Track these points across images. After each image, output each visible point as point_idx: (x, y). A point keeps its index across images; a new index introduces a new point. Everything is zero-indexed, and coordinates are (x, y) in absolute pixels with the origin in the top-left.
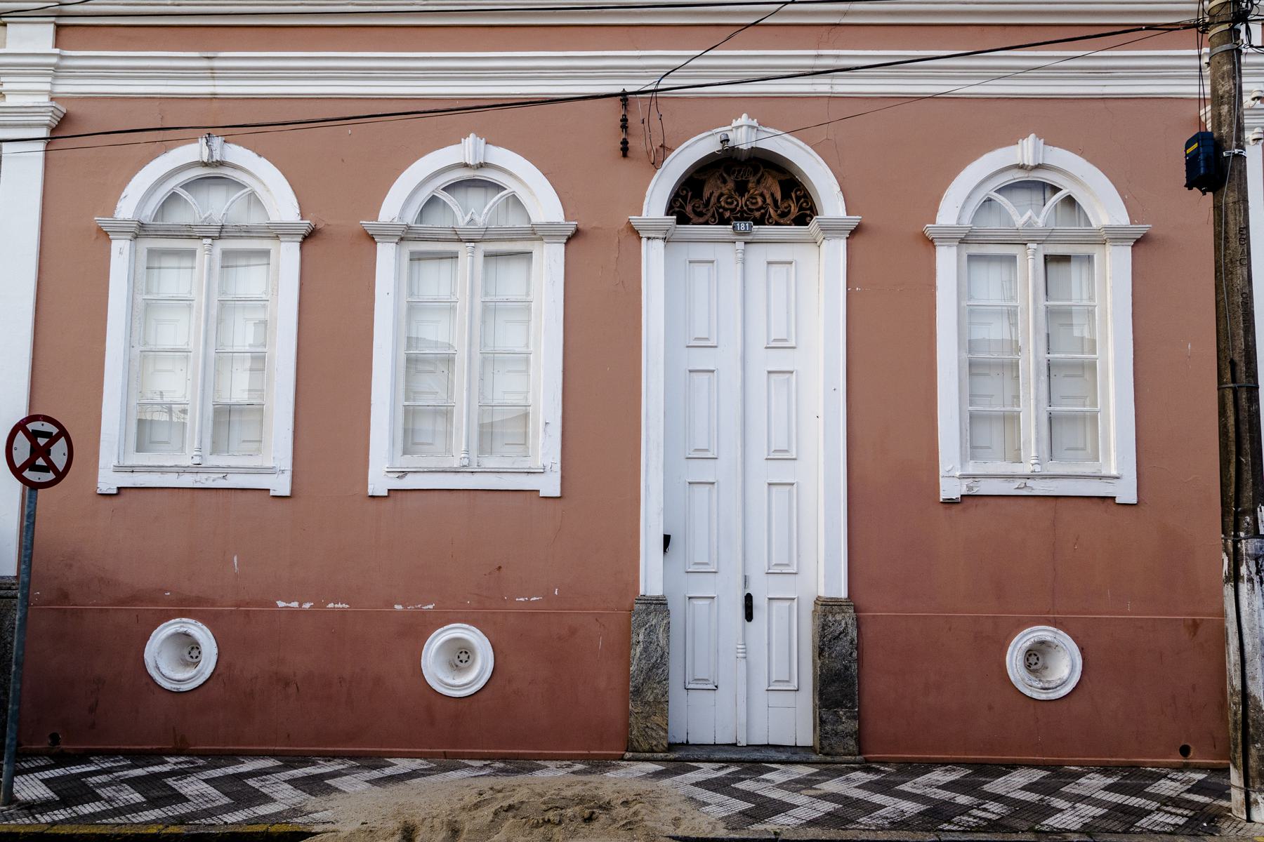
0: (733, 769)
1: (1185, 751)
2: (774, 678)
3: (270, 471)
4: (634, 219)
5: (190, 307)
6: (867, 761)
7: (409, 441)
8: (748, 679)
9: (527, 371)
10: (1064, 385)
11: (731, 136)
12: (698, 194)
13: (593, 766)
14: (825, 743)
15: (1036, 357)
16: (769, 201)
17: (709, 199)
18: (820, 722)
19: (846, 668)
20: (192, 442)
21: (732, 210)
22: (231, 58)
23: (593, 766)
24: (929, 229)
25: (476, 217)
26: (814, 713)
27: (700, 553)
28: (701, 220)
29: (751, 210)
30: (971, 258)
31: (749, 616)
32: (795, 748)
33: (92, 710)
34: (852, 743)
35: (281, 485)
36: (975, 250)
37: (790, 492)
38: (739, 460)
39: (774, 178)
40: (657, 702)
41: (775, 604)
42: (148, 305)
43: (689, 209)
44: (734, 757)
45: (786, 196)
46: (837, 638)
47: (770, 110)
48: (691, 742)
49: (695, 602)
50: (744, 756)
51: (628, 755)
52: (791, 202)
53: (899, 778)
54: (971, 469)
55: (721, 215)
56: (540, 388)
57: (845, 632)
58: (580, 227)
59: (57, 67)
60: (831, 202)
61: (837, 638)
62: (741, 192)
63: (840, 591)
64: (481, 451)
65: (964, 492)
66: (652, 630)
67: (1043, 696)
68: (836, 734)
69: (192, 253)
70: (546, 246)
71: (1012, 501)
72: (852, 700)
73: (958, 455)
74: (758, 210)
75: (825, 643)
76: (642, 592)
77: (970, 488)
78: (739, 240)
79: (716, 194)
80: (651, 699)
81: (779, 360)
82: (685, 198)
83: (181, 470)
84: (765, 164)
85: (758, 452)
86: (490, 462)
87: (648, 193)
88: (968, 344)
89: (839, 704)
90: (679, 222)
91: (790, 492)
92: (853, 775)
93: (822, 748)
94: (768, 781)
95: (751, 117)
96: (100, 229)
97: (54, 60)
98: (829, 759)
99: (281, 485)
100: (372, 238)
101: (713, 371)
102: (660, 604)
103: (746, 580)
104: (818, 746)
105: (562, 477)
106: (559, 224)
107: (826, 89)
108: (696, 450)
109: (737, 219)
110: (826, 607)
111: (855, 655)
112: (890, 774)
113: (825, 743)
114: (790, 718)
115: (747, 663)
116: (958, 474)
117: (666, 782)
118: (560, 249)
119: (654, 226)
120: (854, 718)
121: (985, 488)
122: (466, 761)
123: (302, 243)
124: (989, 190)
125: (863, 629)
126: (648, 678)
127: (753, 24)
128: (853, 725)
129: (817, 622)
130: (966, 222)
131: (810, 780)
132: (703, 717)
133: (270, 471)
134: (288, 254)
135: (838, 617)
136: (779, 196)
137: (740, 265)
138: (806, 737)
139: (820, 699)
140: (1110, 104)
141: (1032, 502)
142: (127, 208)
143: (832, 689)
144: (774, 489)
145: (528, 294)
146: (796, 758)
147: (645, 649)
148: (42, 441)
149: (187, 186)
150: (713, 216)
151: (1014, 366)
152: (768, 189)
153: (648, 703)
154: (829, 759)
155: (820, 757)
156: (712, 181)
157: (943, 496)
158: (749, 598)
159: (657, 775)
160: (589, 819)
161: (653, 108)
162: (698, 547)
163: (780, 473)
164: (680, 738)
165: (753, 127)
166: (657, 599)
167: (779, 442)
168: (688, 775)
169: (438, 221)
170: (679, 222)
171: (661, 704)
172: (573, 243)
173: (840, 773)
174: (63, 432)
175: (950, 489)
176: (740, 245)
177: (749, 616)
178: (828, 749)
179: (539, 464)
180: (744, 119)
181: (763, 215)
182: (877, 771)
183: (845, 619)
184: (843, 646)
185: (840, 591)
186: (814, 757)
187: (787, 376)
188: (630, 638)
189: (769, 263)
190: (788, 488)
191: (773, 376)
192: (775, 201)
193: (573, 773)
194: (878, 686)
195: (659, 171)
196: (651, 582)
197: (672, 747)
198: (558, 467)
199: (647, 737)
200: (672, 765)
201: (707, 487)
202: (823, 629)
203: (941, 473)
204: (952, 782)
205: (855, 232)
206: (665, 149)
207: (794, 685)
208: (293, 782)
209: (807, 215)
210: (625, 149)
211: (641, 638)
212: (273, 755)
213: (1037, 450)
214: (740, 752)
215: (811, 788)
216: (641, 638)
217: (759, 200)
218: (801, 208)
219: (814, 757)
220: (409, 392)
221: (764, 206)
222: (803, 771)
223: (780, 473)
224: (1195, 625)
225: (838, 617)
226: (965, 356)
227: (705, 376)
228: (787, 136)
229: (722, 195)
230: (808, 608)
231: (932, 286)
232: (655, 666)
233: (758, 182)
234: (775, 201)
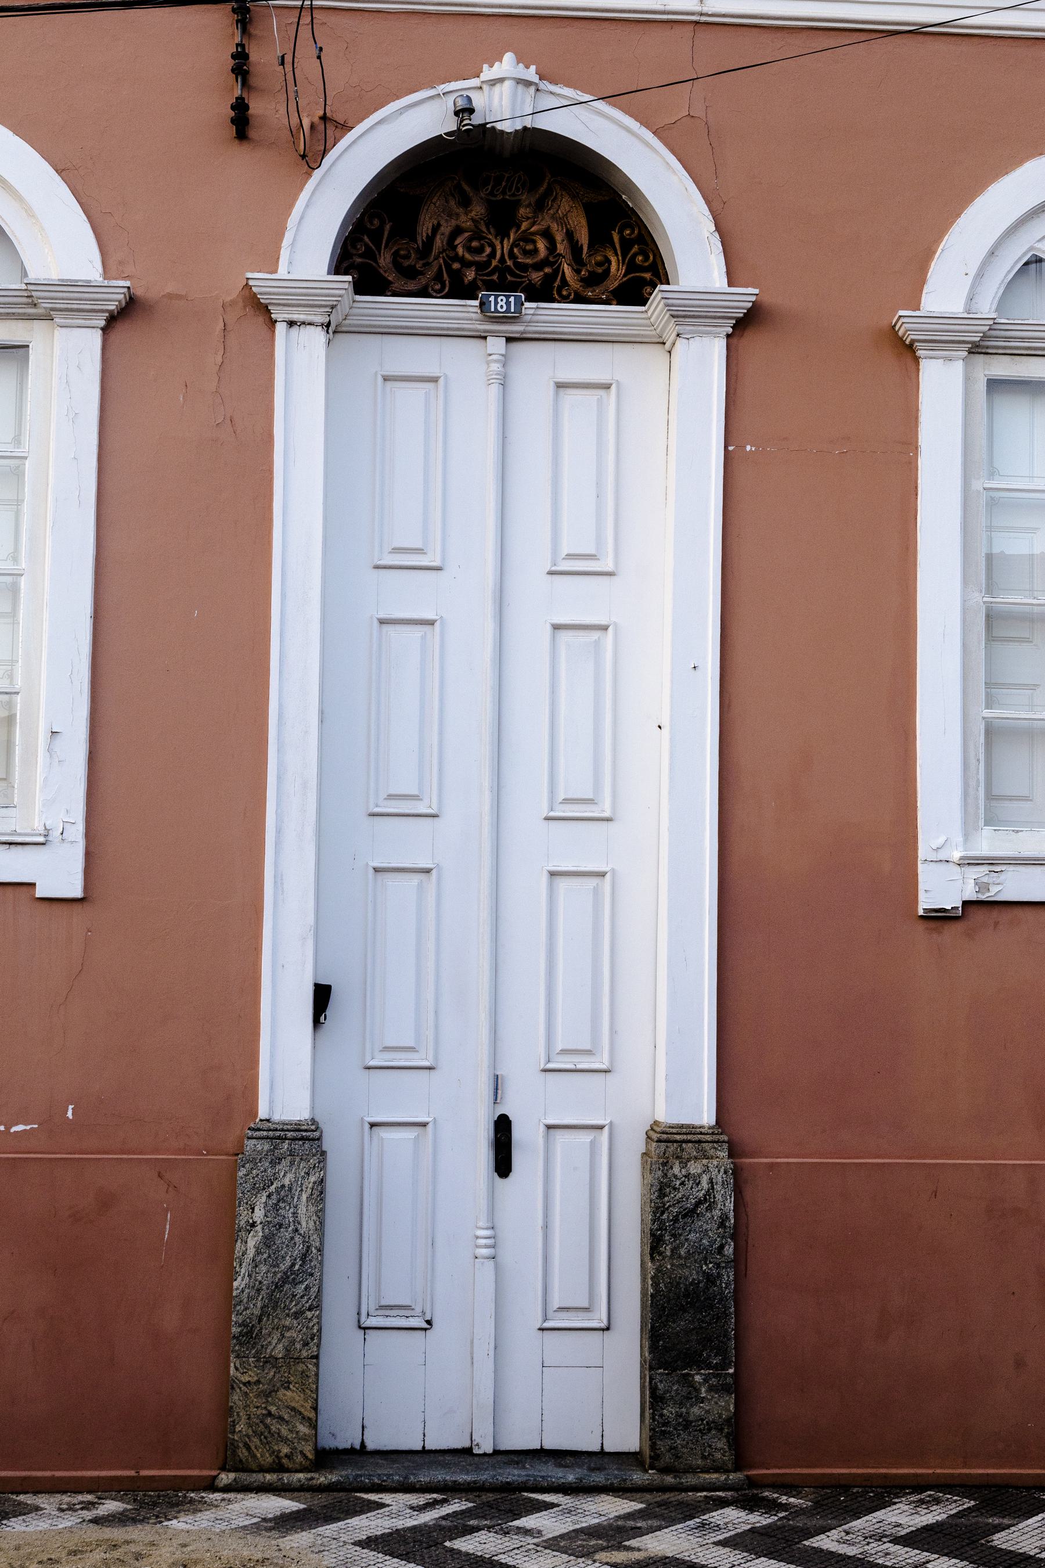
0: (456, 1506)
2: (556, 1302)
4: (259, 280)
6: (752, 1483)
7: (991, 802)
8: (496, 1306)
9: (14, 614)
10: (1023, 661)
11: (478, 101)
12: (406, 228)
13: (142, 1505)
14: (662, 1445)
16: (561, 248)
17: (431, 239)
18: (654, 1399)
19: (711, 1279)
21: (481, 267)
23: (142, 1505)
24: (907, 323)
26: (642, 1377)
27: (398, 1030)
28: (412, 286)
29: (524, 268)
30: (995, 385)
31: (503, 1165)
32: (601, 1457)
34: (721, 1444)
35: (60, 874)
36: (1003, 368)
37: (596, 892)
38: (487, 819)
39: (574, 197)
40: (291, 1358)
41: (561, 1138)
43: (385, 260)
44: (463, 1478)
45: (599, 238)
46: (691, 1213)
48: (371, 1446)
49: (384, 1133)
50: (484, 1477)
51: (226, 1478)
52: (618, 256)
53: (817, 1521)
54: (987, 844)
55: (456, 277)
57: (708, 1200)
58: (139, 292)
60: (696, 258)
61: (691, 1213)
62: (498, 228)
63: (702, 1111)
65: (970, 894)
66: (283, 1197)
68: (687, 1425)
70: (59, 333)
72: (722, 1351)
73: (957, 814)
74: (538, 267)
75: (667, 1222)
76: (263, 1113)
77: (982, 887)
78: (496, 334)
79: (446, 229)
80: (279, 1351)
81: (578, 602)
82: (376, 236)
85: (528, 803)
87: (292, 221)
88: (987, 569)
89: (695, 1361)
90: (361, 288)
91: (596, 892)
92: (716, 1517)
93: (655, 1457)
94: (527, 1532)
95: (523, 59)
98: (669, 1479)
100: (911, 348)
101: (431, 623)
102: (304, 1140)
103: (497, 1085)
104: (647, 1452)
105: (88, 855)
106: (88, 284)
108: (391, 797)
109: (492, 287)
110: (670, 1144)
111: (729, 1250)
112: (800, 1512)
113: (662, 1445)
114: (590, 1392)
115: (497, 1268)
116: (956, 855)
117: (300, 1539)
118: (95, 338)
119: (304, 296)
120: (725, 1389)
121: (1015, 886)
122: (373, 1497)
123: (104, 329)
125: (748, 1194)
126: (272, 1304)
128: (724, 1405)
129: (649, 1178)
130: (986, 307)
131: (620, 1530)
132: (396, 1391)
135: (694, 1168)
136: (583, 237)
137: (495, 389)
138: (626, 1434)
139: (653, 1348)
143: (680, 1325)
144: (563, 884)
145: (17, 440)
146: (598, 1478)
147: (268, 1241)
150: (438, 277)
152: (562, 221)
153: (271, 1361)
154: (669, 1479)
155: (649, 1476)
156: (438, 201)
157: (925, 902)
158: (503, 1127)
159: (285, 1523)
161: (305, 32)
162: (390, 1010)
163: (576, 848)
164: (347, 1438)
165: (528, 84)
166: (297, 1127)
167: (575, 780)
168: (355, 1521)
170: (361, 288)
171: (303, 1364)
173: (687, 1512)
175: (940, 888)
176: (496, 345)
177: (503, 1165)
178: (667, 1459)
180: (507, 65)
181: (549, 279)
182: (772, 1506)
183: (711, 1172)
184: (705, 1230)
185: (702, 1111)
186: (638, 1477)
187: (595, 635)
188: (234, 1216)
189: (560, 386)
190: (593, 882)
191: (564, 636)
192: (575, 249)
193: (96, 1521)
194: (779, 1317)
195: (317, 174)
196: (286, 1084)
197: (326, 1458)
198: (77, 832)
199: (267, 1437)
200: (322, 1499)
201: (415, 879)
202: (662, 1194)
203: (923, 852)
204: (927, 1528)
205: (746, 324)
206: (330, 128)
207: (599, 1319)
209: (644, 282)
210: (241, 123)
211: (259, 1215)
214: (478, 1468)
215: (620, 1547)
216: (259, 1215)
217: (541, 245)
218: (632, 267)
219: (638, 1477)
220: (994, 688)
221: (553, 258)
222: (611, 1508)
223: (576, 848)
225: (694, 1168)
226: (978, 599)
228: (600, 105)
229: (458, 231)
230: (633, 1147)
232: (289, 1278)
233: (540, 207)
234: (575, 249)
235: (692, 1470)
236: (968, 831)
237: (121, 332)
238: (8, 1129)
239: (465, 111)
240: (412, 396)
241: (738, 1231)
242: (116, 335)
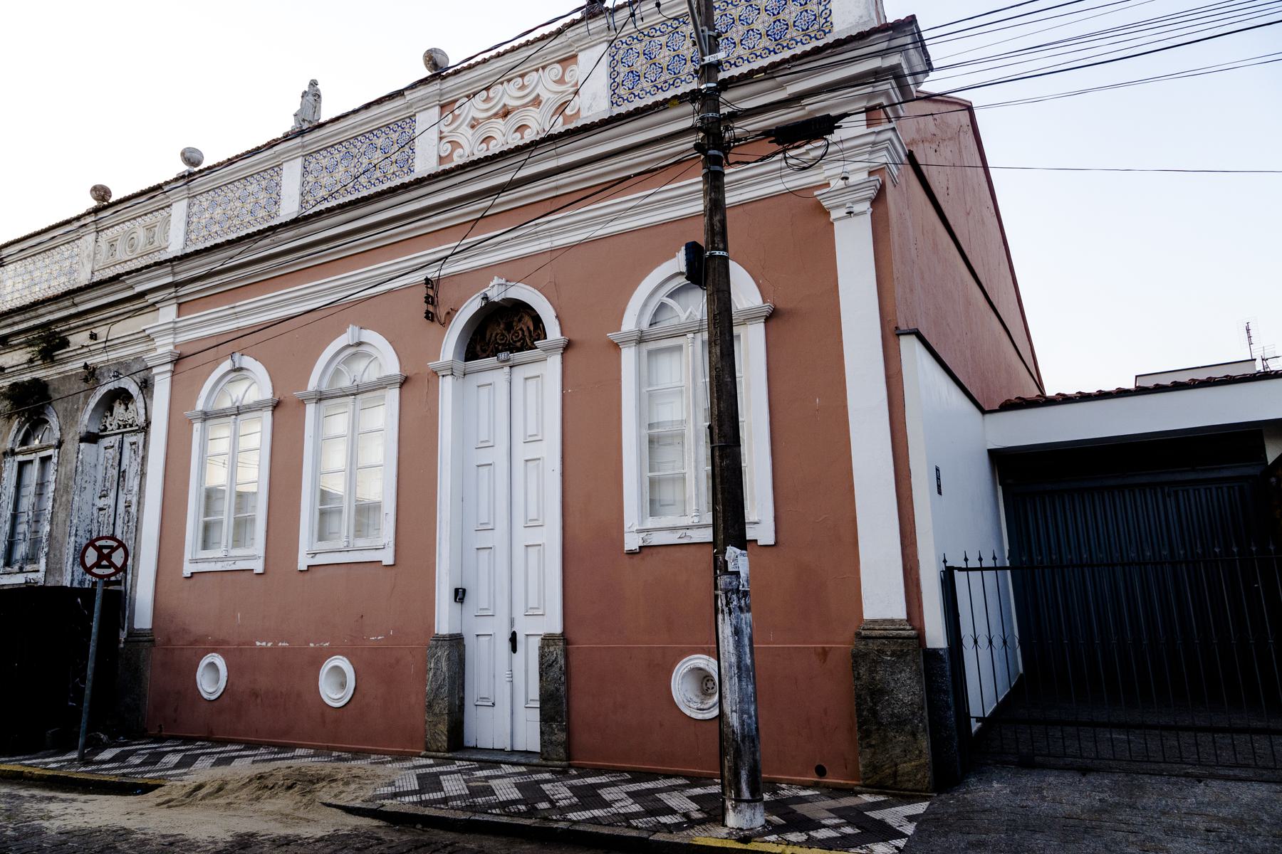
1: (821, 771)
3: (253, 557)
5: (681, 392)
7: (654, 507)
11: (489, 294)
15: (695, 425)
19: (558, 690)
30: (650, 353)
31: (514, 649)
33: (176, 710)
46: (551, 665)
54: (650, 523)
56: (379, 487)
57: (556, 660)
58: (780, 305)
61: (551, 665)
62: (501, 331)
63: (557, 628)
64: (356, 536)
67: (700, 716)
69: (680, 348)
71: (677, 549)
83: (217, 560)
84: (520, 308)
86: (361, 543)
89: (553, 719)
97: (871, 138)
100: (617, 345)
102: (456, 641)
110: (547, 640)
118: (762, 325)
120: (562, 730)
121: (657, 539)
124: (661, 296)
127: (482, 217)
133: (253, 557)
134: (393, 394)
135: (552, 649)
140: (746, 207)
141: (692, 549)
142: (629, 324)
147: (435, 674)
148: (106, 551)
149: (671, 295)
162: (479, 597)
164: (472, 744)
169: (667, 323)
175: (632, 542)
177: (514, 649)
179: (380, 545)
180: (496, 281)
183: (557, 650)
185: (557, 628)
194: (582, 704)
196: (445, 622)
206: (450, 314)
213: (698, 504)
221: (523, 338)
224: (824, 653)
227: (486, 468)
231: (619, 380)
233: (520, 320)
235: (553, 760)
237: (772, 323)
239: (485, 298)
240: (484, 391)
242: (277, 413)
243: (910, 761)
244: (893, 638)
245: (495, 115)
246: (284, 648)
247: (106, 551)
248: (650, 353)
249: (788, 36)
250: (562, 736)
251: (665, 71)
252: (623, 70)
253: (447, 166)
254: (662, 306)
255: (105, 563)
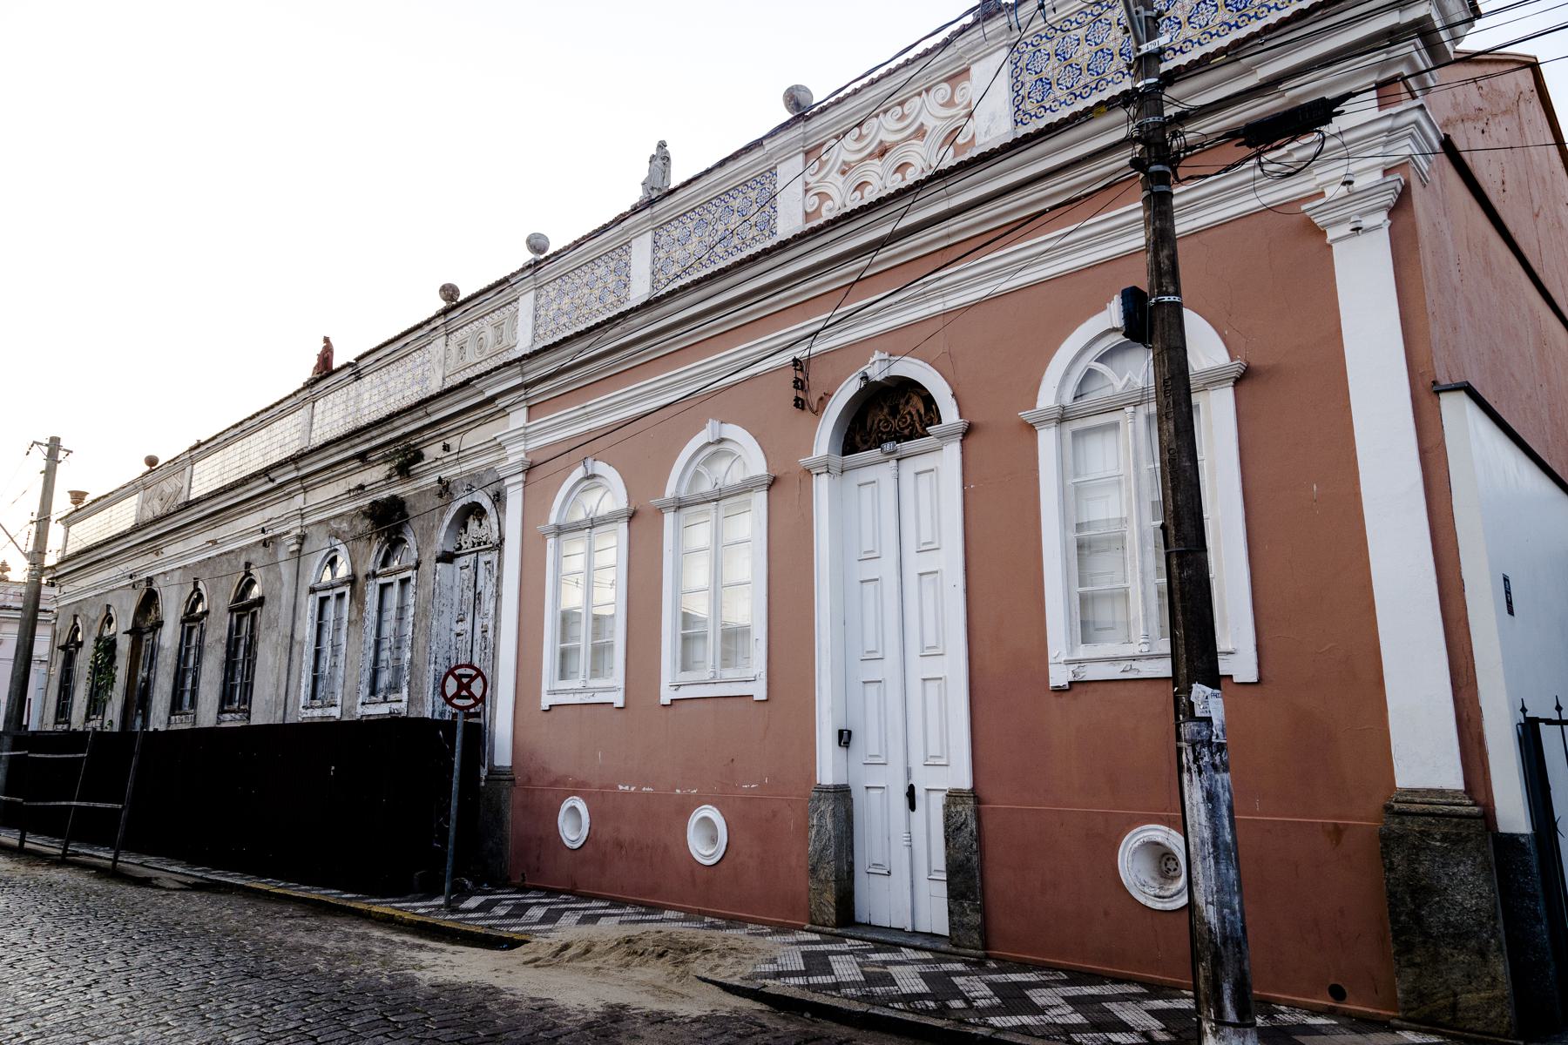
1: (1338, 993)
4: (1026, 415)
5: (1119, 482)
7: (1087, 630)
11: (869, 372)
15: (1140, 525)
19: (969, 860)
20: (1139, 631)
22: (595, 403)
25: (1134, 379)
30: (1075, 434)
31: (912, 807)
35: (760, 692)
36: (1078, 425)
42: (1078, 488)
47: (895, 341)
49: (872, 792)
54: (1083, 652)
56: (747, 608)
58: (1253, 363)
59: (525, 435)
61: (959, 829)
62: (886, 417)
63: (965, 783)
65: (1071, 679)
67: (1159, 905)
71: (1121, 685)
72: (974, 893)
83: (575, 692)
84: (906, 387)
86: (729, 674)
89: (964, 896)
96: (1025, 423)
97: (1388, 124)
99: (760, 692)
100: (1031, 427)
102: (842, 794)
105: (769, 684)
107: (940, 307)
110: (954, 797)
118: (1230, 391)
120: (977, 911)
135: (959, 808)
140: (1201, 236)
141: (1142, 685)
142: (1047, 398)
148: (465, 680)
149: (1101, 359)
151: (1123, 539)
153: (820, 881)
157: (1053, 683)
158: (911, 789)
160: (661, 956)
162: (868, 741)
164: (865, 919)
169: (1096, 395)
172: (773, 489)
174: (480, 673)
175: (1059, 676)
177: (912, 807)
180: (877, 356)
183: (966, 810)
184: (964, 837)
185: (965, 783)
194: (1000, 879)
198: (764, 675)
203: (1050, 660)
206: (824, 400)
208: (1069, 1000)
212: (1142, 984)
213: (1146, 628)
221: (912, 424)
224: (1338, 832)
225: (959, 808)
226: (1072, 536)
233: (907, 403)
235: (965, 947)
236: (1072, 647)
238: (639, 788)
239: (865, 377)
240: (867, 490)
241: (979, 837)
243: (1478, 990)
244: (1444, 815)
245: (870, 155)
246: (648, 794)
247: (465, 680)
248: (1075, 434)
249: (1082, 83)
250: (975, 919)
251: (1085, 72)
252: (1029, 78)
253: (815, 224)
254: (1090, 373)
255: (464, 693)
